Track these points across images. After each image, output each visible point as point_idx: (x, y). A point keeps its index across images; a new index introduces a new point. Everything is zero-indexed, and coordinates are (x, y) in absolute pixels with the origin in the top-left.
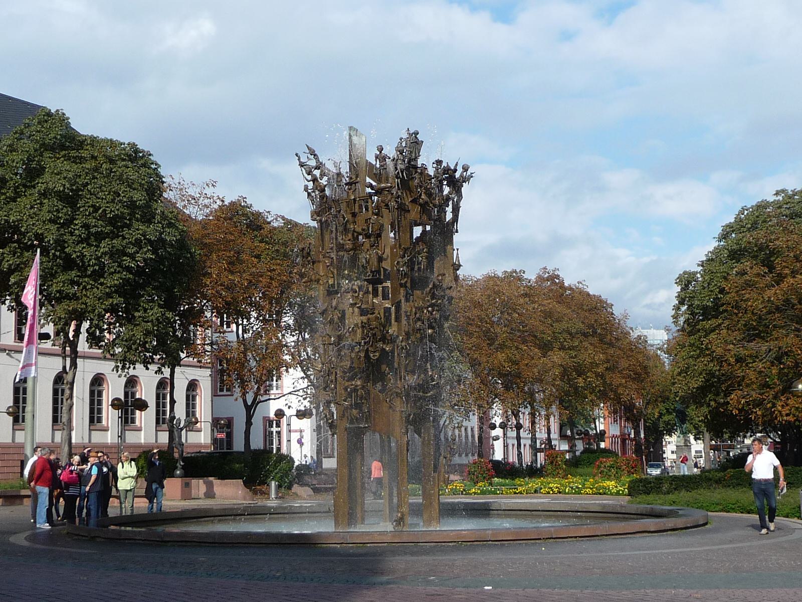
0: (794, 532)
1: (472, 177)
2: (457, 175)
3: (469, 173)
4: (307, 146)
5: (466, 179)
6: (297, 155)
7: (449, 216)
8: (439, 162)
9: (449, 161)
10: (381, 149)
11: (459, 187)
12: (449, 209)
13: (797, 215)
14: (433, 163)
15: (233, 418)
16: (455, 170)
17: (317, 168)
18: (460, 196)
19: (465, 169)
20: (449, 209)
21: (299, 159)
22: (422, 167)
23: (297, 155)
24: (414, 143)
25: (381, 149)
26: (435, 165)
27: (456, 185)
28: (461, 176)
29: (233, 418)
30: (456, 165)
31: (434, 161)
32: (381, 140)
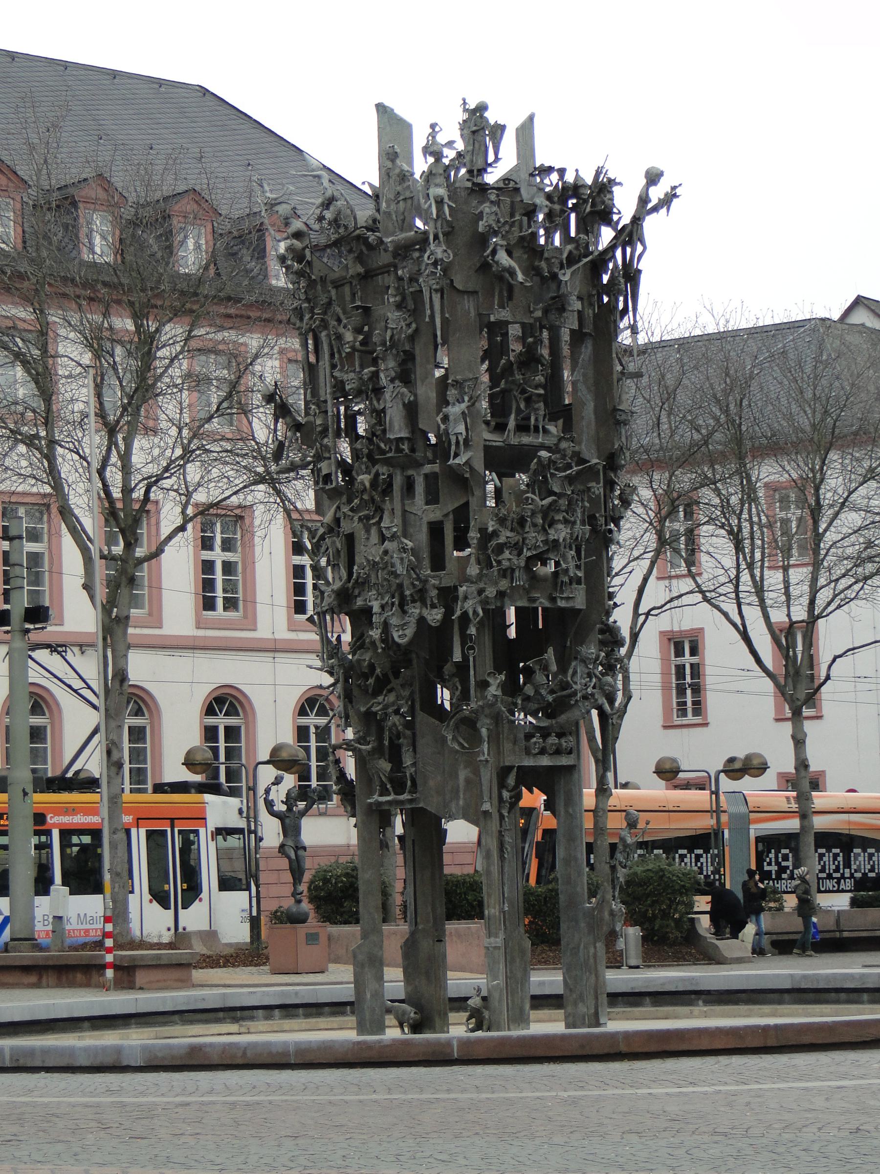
1: (675, 196)
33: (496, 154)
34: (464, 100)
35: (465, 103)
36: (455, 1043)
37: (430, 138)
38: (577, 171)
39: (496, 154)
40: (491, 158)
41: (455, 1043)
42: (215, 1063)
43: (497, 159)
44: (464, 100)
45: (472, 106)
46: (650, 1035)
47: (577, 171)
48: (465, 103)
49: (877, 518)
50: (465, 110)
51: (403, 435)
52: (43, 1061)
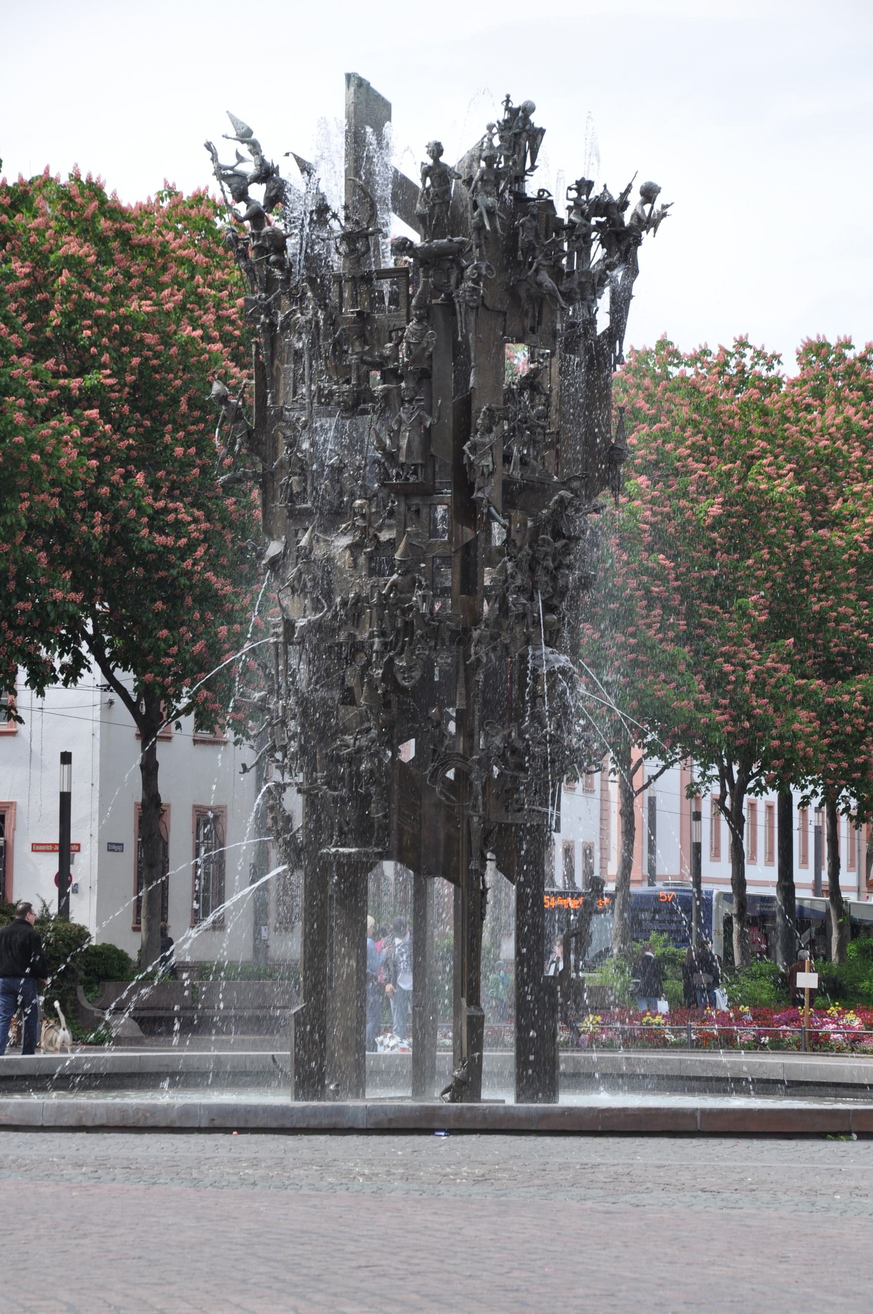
0: (285, 790)
1: (665, 215)
2: (627, 218)
3: (657, 206)
4: (231, 117)
5: (651, 223)
6: (209, 146)
7: (603, 322)
8: (584, 186)
9: (610, 182)
10: (437, 150)
11: (630, 246)
12: (604, 303)
13: (296, 1311)
14: (570, 189)
15: (194, 807)
16: (624, 204)
17: (259, 179)
18: (633, 271)
19: (649, 193)
20: (604, 303)
21: (214, 159)
22: (540, 197)
23: (209, 146)
24: (519, 133)
25: (437, 150)
26: (574, 194)
27: (624, 241)
28: (636, 216)
29: (194, 807)
30: (628, 190)
31: (572, 182)
32: (439, 125)
33: (533, 160)
34: (508, 96)
35: (508, 101)
36: (698, 1115)
37: (486, 139)
38: (605, 186)
39: (533, 160)
40: (528, 165)
41: (698, 1115)
42: (361, 1126)
43: (533, 168)
44: (508, 96)
45: (516, 104)
46: (708, 1114)
47: (605, 186)
48: (508, 101)
49: (2, 370)
50: (508, 109)
51: (420, 461)
52: (246, 1121)
